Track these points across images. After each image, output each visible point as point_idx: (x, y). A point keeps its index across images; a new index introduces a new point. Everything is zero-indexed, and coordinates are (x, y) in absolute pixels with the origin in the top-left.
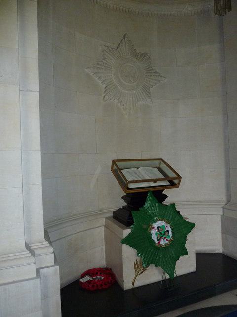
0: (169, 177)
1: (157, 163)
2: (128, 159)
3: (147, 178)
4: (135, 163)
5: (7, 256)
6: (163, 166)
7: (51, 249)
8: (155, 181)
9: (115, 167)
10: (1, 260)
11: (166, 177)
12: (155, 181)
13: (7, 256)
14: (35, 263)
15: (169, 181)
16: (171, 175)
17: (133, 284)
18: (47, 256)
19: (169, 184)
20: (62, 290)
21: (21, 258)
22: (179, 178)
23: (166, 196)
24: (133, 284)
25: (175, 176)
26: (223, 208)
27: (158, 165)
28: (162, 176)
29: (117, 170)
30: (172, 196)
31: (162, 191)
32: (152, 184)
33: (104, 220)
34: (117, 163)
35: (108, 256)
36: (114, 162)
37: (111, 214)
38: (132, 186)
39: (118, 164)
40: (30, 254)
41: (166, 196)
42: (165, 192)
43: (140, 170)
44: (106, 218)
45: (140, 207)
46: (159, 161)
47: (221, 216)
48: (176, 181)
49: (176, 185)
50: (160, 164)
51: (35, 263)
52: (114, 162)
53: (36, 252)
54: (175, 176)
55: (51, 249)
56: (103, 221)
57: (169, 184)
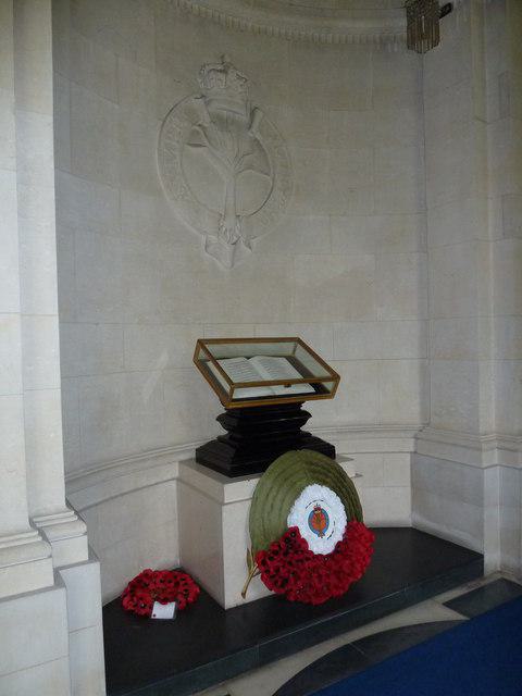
0: (312, 376)
1: (288, 348)
2: (238, 337)
3: (267, 377)
4: (239, 346)
5: (18, 537)
6: (301, 355)
7: (83, 528)
8: (288, 384)
9: (202, 355)
10: (3, 546)
11: (307, 376)
12: (288, 384)
13: (18, 537)
14: (50, 556)
15: (314, 385)
16: (318, 371)
17: (244, 594)
18: (74, 543)
19: (313, 390)
20: (104, 609)
21: (11, 547)
22: (335, 378)
23: (307, 415)
24: (244, 594)
25: (326, 374)
26: (416, 438)
27: (290, 353)
28: (298, 376)
29: (206, 358)
30: (321, 419)
31: (300, 404)
32: (280, 390)
33: (177, 468)
34: (208, 347)
35: (185, 545)
36: (201, 343)
37: (193, 455)
38: (240, 394)
39: (210, 347)
40: (40, 539)
41: (307, 415)
42: (307, 406)
43: (254, 361)
44: (181, 462)
45: (220, 439)
46: (292, 344)
47: (179, 480)
48: (329, 385)
49: (328, 392)
50: (295, 350)
51: (50, 556)
52: (201, 343)
53: (50, 534)
54: (326, 374)
55: (83, 528)
56: (174, 471)
57: (313, 390)
